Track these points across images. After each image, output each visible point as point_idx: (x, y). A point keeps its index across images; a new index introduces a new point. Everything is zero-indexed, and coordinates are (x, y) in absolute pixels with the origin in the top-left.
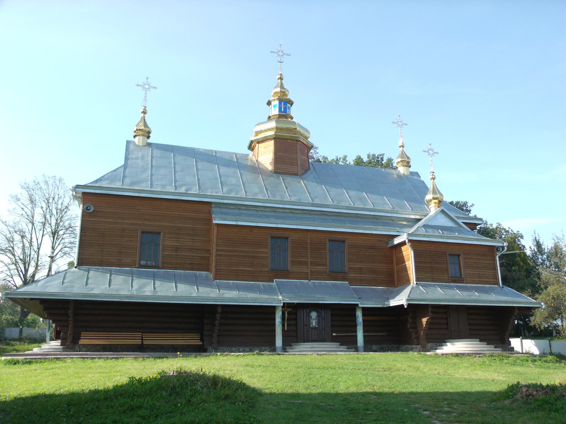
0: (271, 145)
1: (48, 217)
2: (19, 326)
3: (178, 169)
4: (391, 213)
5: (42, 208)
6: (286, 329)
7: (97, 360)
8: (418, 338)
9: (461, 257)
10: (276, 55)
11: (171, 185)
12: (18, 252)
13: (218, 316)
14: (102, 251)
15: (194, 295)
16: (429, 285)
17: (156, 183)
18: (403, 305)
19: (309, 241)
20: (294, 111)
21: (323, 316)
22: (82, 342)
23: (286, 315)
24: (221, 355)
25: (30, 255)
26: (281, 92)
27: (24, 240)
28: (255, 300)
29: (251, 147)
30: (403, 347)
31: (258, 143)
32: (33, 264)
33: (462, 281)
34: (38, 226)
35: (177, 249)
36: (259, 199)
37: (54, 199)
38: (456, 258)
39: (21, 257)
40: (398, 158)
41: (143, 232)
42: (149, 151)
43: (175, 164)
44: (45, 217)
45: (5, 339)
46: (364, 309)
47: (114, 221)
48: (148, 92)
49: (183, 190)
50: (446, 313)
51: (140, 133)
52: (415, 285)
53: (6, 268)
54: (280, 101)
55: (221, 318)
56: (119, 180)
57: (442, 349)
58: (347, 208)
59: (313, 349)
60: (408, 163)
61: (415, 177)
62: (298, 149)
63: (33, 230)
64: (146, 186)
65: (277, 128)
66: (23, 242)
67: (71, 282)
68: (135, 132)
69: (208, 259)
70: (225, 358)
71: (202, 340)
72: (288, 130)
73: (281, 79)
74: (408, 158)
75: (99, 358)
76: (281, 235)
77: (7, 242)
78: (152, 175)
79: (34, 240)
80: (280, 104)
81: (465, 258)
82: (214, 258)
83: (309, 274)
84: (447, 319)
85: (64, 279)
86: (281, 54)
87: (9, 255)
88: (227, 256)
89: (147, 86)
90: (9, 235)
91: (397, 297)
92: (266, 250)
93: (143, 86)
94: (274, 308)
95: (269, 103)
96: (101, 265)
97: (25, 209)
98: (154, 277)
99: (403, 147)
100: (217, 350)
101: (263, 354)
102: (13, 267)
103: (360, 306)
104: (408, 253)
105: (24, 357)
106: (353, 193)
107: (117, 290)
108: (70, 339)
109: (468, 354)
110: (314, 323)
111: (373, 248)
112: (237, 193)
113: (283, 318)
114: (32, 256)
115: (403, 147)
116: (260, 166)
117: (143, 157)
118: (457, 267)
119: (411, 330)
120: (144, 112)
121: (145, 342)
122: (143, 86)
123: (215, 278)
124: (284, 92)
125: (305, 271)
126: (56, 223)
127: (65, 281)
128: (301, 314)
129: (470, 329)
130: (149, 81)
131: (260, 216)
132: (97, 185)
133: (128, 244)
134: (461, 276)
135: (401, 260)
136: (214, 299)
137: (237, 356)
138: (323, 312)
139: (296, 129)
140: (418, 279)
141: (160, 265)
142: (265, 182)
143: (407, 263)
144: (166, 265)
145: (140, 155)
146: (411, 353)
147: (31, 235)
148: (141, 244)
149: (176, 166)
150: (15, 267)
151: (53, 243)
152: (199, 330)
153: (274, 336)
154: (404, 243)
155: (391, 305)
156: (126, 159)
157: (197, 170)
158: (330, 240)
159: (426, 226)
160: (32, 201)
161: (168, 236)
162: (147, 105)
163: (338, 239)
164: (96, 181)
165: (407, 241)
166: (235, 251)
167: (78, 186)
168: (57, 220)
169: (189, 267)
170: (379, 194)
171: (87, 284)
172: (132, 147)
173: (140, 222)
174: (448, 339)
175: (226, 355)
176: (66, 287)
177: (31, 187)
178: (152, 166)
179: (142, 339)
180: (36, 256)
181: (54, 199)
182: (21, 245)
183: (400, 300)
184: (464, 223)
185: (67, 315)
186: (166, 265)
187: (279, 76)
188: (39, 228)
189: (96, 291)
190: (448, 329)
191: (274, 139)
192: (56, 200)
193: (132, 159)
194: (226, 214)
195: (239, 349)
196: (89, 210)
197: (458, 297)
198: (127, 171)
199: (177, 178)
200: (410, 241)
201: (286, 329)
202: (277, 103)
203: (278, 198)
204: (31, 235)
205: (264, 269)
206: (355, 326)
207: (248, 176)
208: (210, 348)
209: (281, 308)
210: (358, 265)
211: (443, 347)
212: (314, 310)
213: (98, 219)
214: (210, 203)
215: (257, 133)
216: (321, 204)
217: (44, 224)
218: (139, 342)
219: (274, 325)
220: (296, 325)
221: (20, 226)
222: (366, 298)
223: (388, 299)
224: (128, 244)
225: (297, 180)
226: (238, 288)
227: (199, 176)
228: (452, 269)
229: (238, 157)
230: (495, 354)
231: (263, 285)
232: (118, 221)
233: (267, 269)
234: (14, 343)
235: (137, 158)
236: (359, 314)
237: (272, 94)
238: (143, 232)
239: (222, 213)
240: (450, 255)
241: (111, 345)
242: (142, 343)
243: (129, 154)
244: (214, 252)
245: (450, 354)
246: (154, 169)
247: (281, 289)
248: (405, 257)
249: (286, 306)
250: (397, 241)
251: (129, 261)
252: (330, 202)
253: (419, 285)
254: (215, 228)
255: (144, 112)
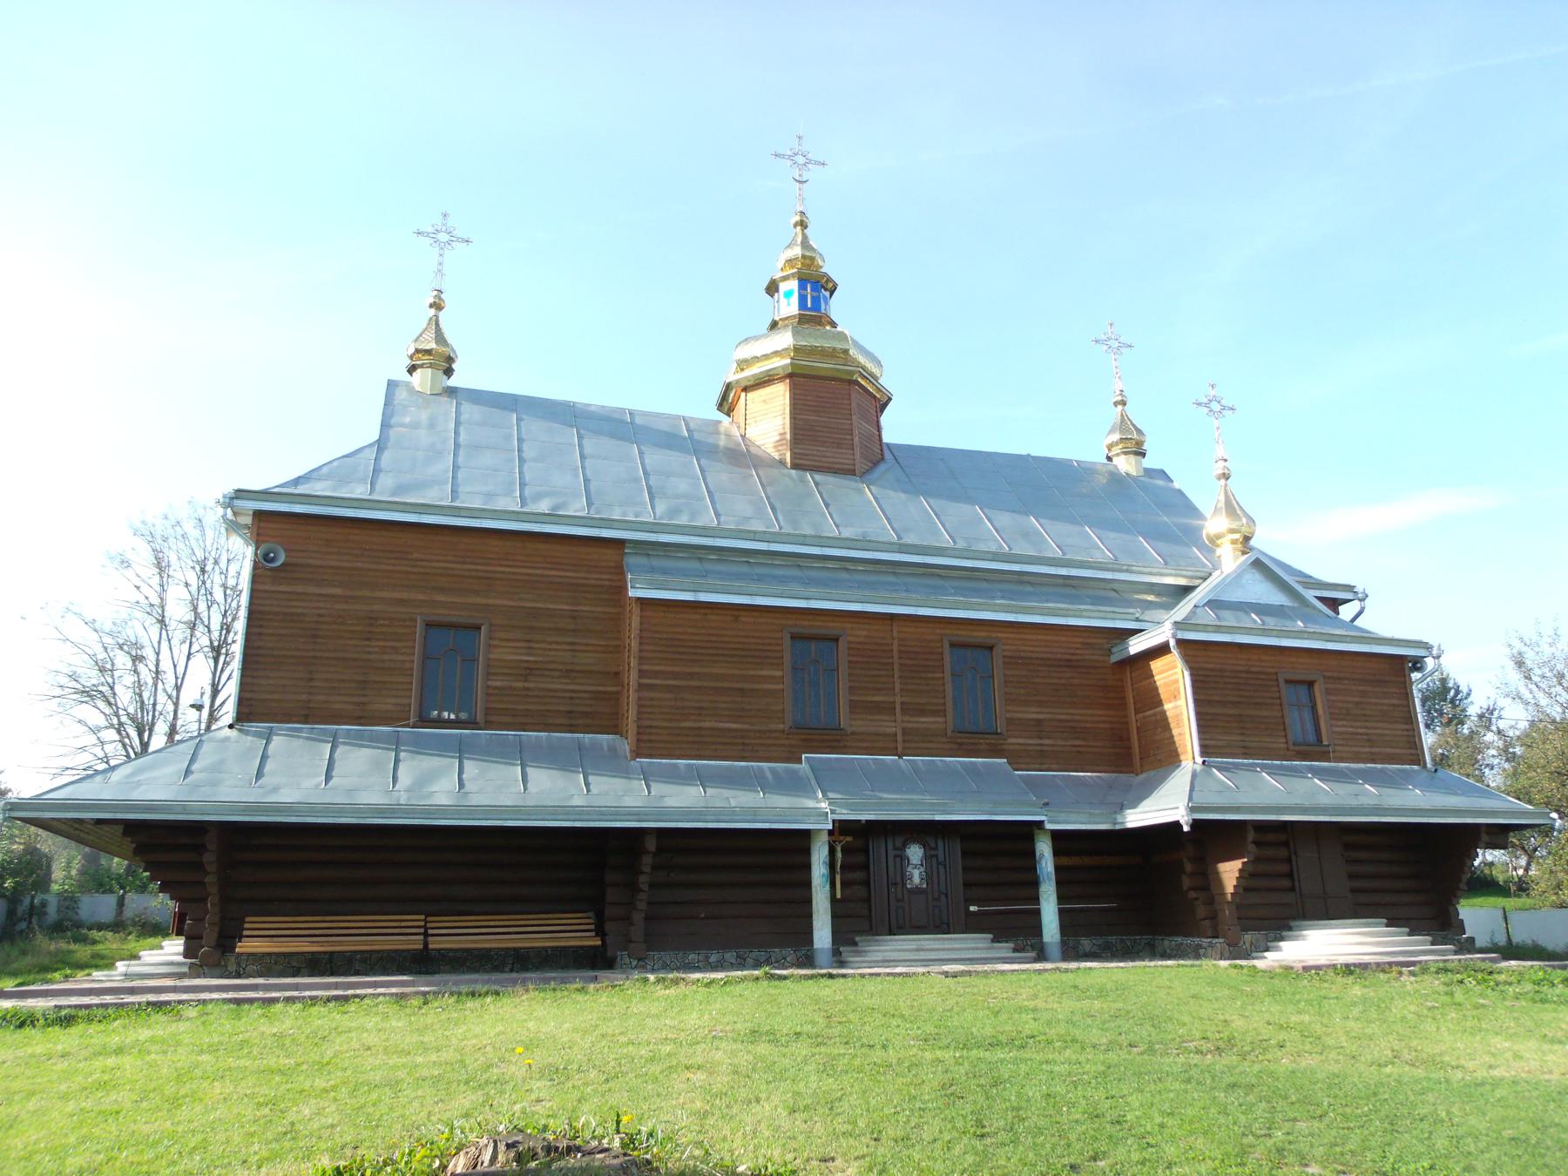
0: (780, 395)
1: (202, 607)
2: (111, 891)
3: (528, 453)
4: (1113, 570)
5: (187, 585)
6: (839, 896)
7: (279, 1006)
8: (1213, 917)
9: (1316, 687)
10: (789, 163)
11: (509, 493)
12: (125, 697)
13: (647, 861)
14: (311, 679)
15: (577, 801)
16: (1236, 766)
17: (468, 489)
18: (1177, 825)
19: (895, 648)
20: (837, 308)
21: (941, 858)
22: (245, 946)
23: (839, 855)
24: (658, 981)
25: (154, 705)
26: (804, 257)
27: (141, 667)
28: (754, 813)
29: (726, 404)
30: (1168, 943)
31: (745, 389)
32: (161, 728)
33: (1324, 756)
34: (179, 633)
35: (528, 671)
36: (755, 532)
37: (216, 562)
38: (1302, 691)
39: (131, 710)
40: (1111, 431)
41: (429, 625)
42: (449, 406)
43: (520, 440)
44: (195, 609)
45: (79, 925)
46: (1057, 836)
47: (341, 597)
48: (447, 252)
49: (544, 506)
50: (1286, 844)
51: (426, 359)
52: (1198, 767)
53: (93, 739)
54: (803, 281)
55: (655, 868)
56: (363, 481)
57: (1278, 949)
58: (996, 557)
59: (923, 955)
60: (1139, 444)
61: (1160, 482)
62: (854, 405)
63: (165, 644)
64: (437, 495)
65: (797, 349)
66: (136, 671)
67: (217, 768)
68: (411, 357)
69: (615, 699)
70: (672, 991)
71: (600, 932)
72: (831, 354)
73: (803, 224)
74: (1139, 431)
75: (288, 1000)
76: (822, 631)
77: (95, 673)
78: (456, 467)
79: (166, 665)
80: (802, 287)
81: (1328, 692)
82: (633, 695)
83: (899, 738)
84: (1289, 860)
85: (192, 761)
86: (800, 160)
87: (101, 705)
88: (669, 689)
89: (444, 237)
90: (102, 655)
91: (1145, 802)
92: (779, 673)
93: (433, 235)
94: (806, 834)
95: (772, 289)
96: (306, 719)
97: (144, 588)
98: (462, 751)
99: (1124, 403)
100: (642, 963)
101: (785, 978)
102: (112, 735)
103: (1049, 826)
104: (1174, 682)
105: (52, 1002)
106: (1005, 519)
107: (350, 791)
108: (210, 934)
109: (1378, 964)
110: (916, 877)
111: (1069, 664)
112: (693, 516)
113: (832, 865)
114: (159, 708)
115: (1124, 403)
116: (753, 450)
117: (432, 425)
118: (1307, 716)
119: (1193, 894)
120: (437, 306)
121: (435, 943)
122: (433, 235)
123: (637, 753)
124: (812, 259)
125: (888, 730)
126: (222, 624)
127: (194, 767)
128: (880, 850)
129: (1353, 891)
130: (450, 223)
131: (760, 579)
132: (301, 490)
133: (386, 657)
134: (1320, 740)
135: (1151, 699)
136: (637, 815)
137: (709, 985)
138: (940, 844)
139: (846, 351)
140: (1205, 750)
141: (480, 718)
142: (769, 489)
143: (1166, 707)
144: (494, 718)
145: (424, 416)
146: (1207, 963)
147: (158, 654)
148: (426, 657)
149: (525, 447)
150: (117, 737)
151: (214, 674)
152: (593, 903)
153: (809, 916)
154: (1161, 650)
155: (1130, 825)
156: (385, 425)
157: (583, 457)
158: (952, 645)
159: (1214, 604)
160: (161, 566)
161: (503, 635)
162: (443, 288)
163: (974, 642)
164: (297, 481)
165: (1172, 643)
166: (691, 676)
167: (240, 494)
168: (224, 616)
169: (562, 721)
170: (1073, 521)
171: (260, 774)
172: (401, 395)
173: (421, 597)
174: (1294, 918)
175: (676, 982)
176: (197, 786)
177: (158, 533)
178: (457, 445)
179: (426, 935)
180: (171, 708)
181: (216, 562)
182: (129, 679)
183: (1165, 805)
184: (1320, 599)
185: (200, 866)
186: (494, 718)
187: (798, 218)
188: (181, 637)
189: (287, 796)
190: (1292, 889)
191: (790, 376)
192: (223, 564)
193: (402, 425)
194: (664, 571)
195: (707, 958)
196: (272, 560)
197: (1324, 801)
198: (386, 456)
199: (527, 478)
200: (1181, 643)
201: (839, 896)
202: (793, 285)
203: (808, 530)
204: (158, 654)
205: (773, 726)
206: (1035, 884)
207: (721, 475)
208: (623, 957)
209: (825, 837)
210: (1031, 713)
211: (1282, 944)
212: (915, 841)
213: (300, 589)
214: (620, 543)
215: (743, 364)
216: (929, 547)
217: (193, 627)
218: (415, 943)
219: (807, 884)
220: (867, 883)
221: (130, 632)
222: (1065, 805)
223: (1122, 808)
224: (386, 657)
225: (853, 484)
226: (704, 779)
227: (588, 473)
228: (1299, 725)
229: (692, 426)
230: (1450, 966)
231: (772, 770)
232: (359, 593)
233: (781, 726)
234: (95, 934)
235: (415, 426)
236: (1044, 849)
237: (780, 264)
238: (429, 625)
239: (653, 570)
240: (1287, 682)
241: (332, 953)
242: (426, 944)
243: (392, 416)
244: (633, 677)
245: (1328, 966)
246: (462, 452)
247: (824, 779)
248: (1161, 691)
249: (842, 828)
250: (1136, 646)
251: (389, 707)
252: (945, 540)
253: (1210, 766)
254: (636, 610)
255: (437, 306)
